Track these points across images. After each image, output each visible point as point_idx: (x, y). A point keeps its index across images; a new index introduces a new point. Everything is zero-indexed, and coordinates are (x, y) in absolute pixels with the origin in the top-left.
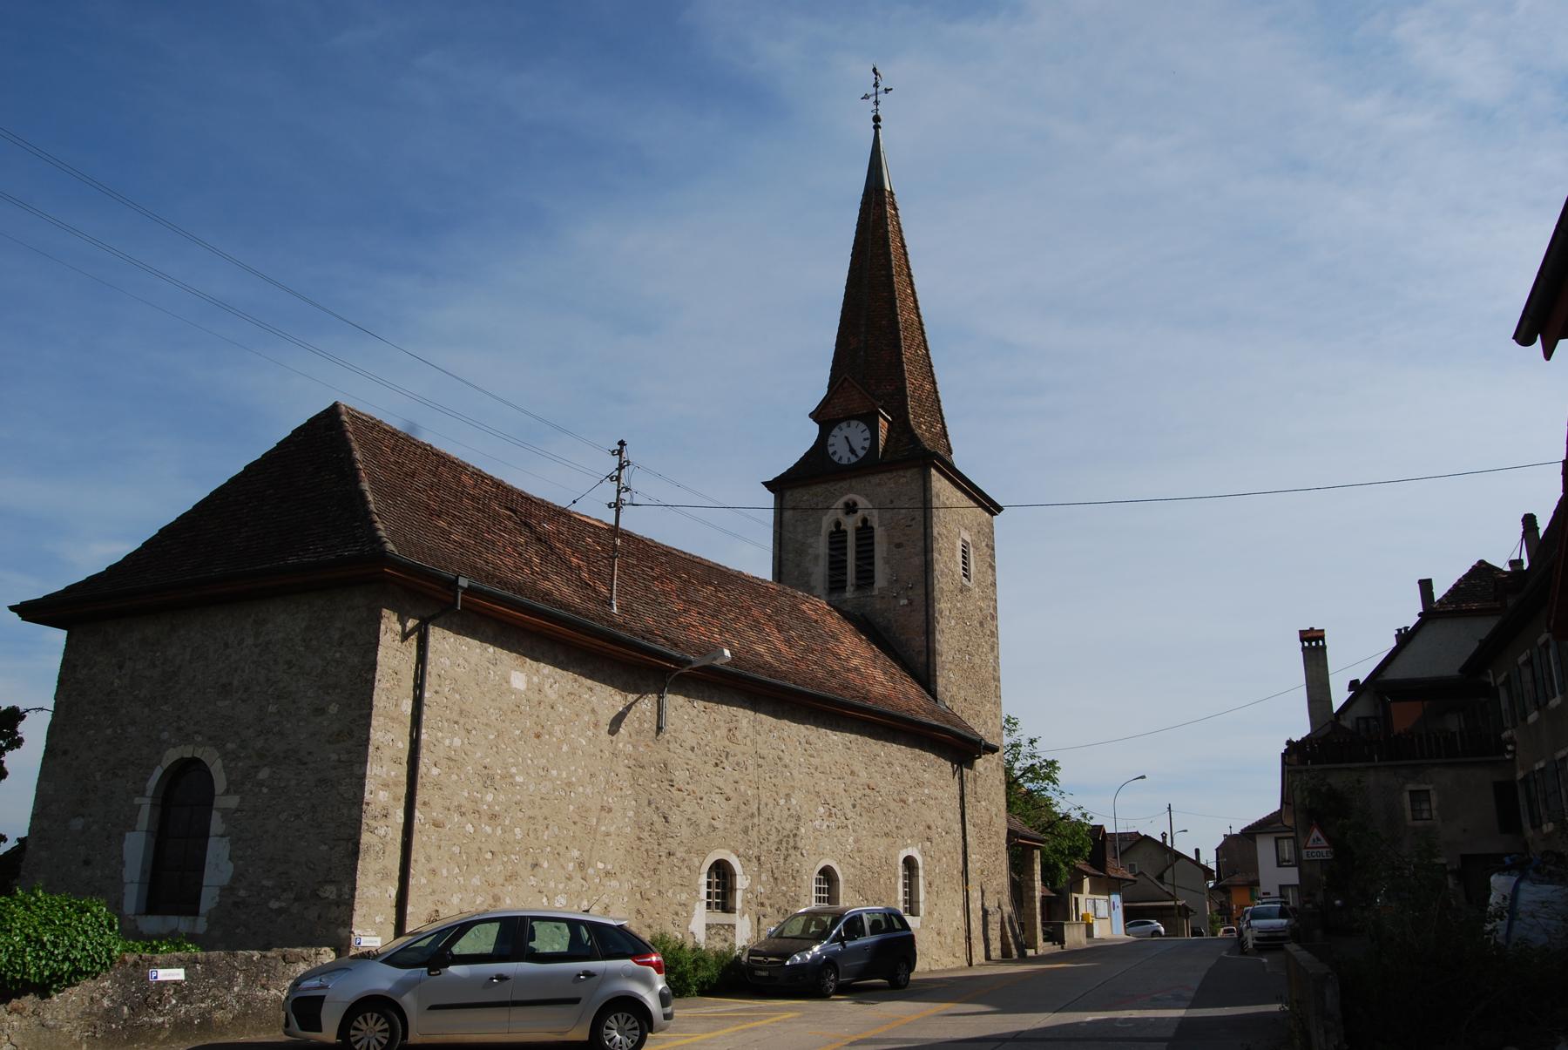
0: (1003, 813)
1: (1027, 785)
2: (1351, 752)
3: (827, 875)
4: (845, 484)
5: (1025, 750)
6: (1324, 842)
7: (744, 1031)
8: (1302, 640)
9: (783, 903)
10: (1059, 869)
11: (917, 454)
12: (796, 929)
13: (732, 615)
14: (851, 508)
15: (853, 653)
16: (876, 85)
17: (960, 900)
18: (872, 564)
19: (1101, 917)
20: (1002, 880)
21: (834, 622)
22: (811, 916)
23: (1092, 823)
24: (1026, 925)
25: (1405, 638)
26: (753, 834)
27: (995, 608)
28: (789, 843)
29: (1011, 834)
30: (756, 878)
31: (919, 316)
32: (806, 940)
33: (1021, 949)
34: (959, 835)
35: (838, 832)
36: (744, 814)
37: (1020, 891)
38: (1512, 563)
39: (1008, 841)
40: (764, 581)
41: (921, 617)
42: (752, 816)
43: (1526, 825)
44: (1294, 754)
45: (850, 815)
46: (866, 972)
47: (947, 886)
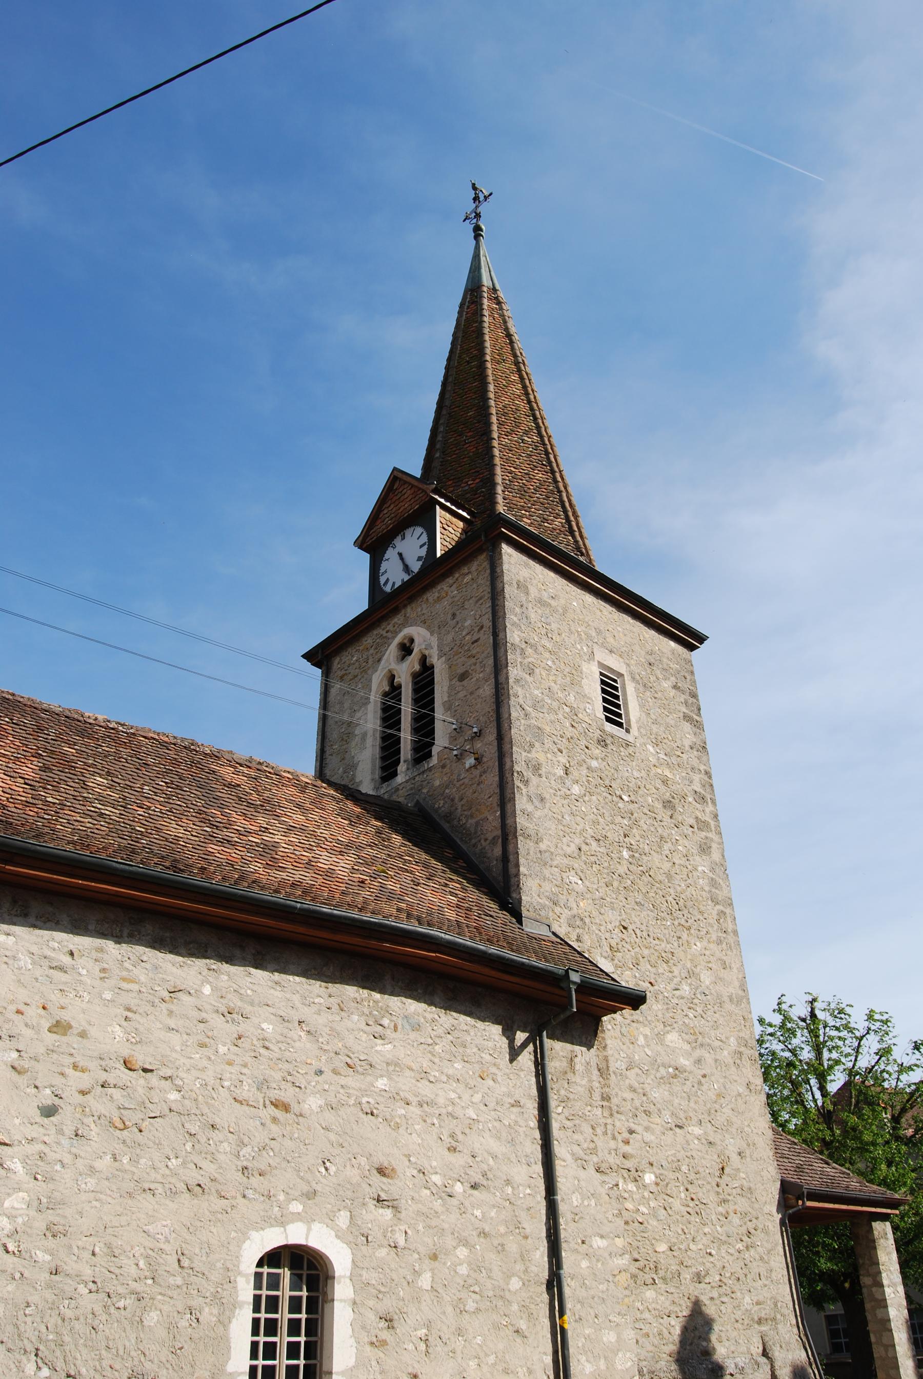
14: (406, 649)
39: (784, 1204)
41: (492, 779)
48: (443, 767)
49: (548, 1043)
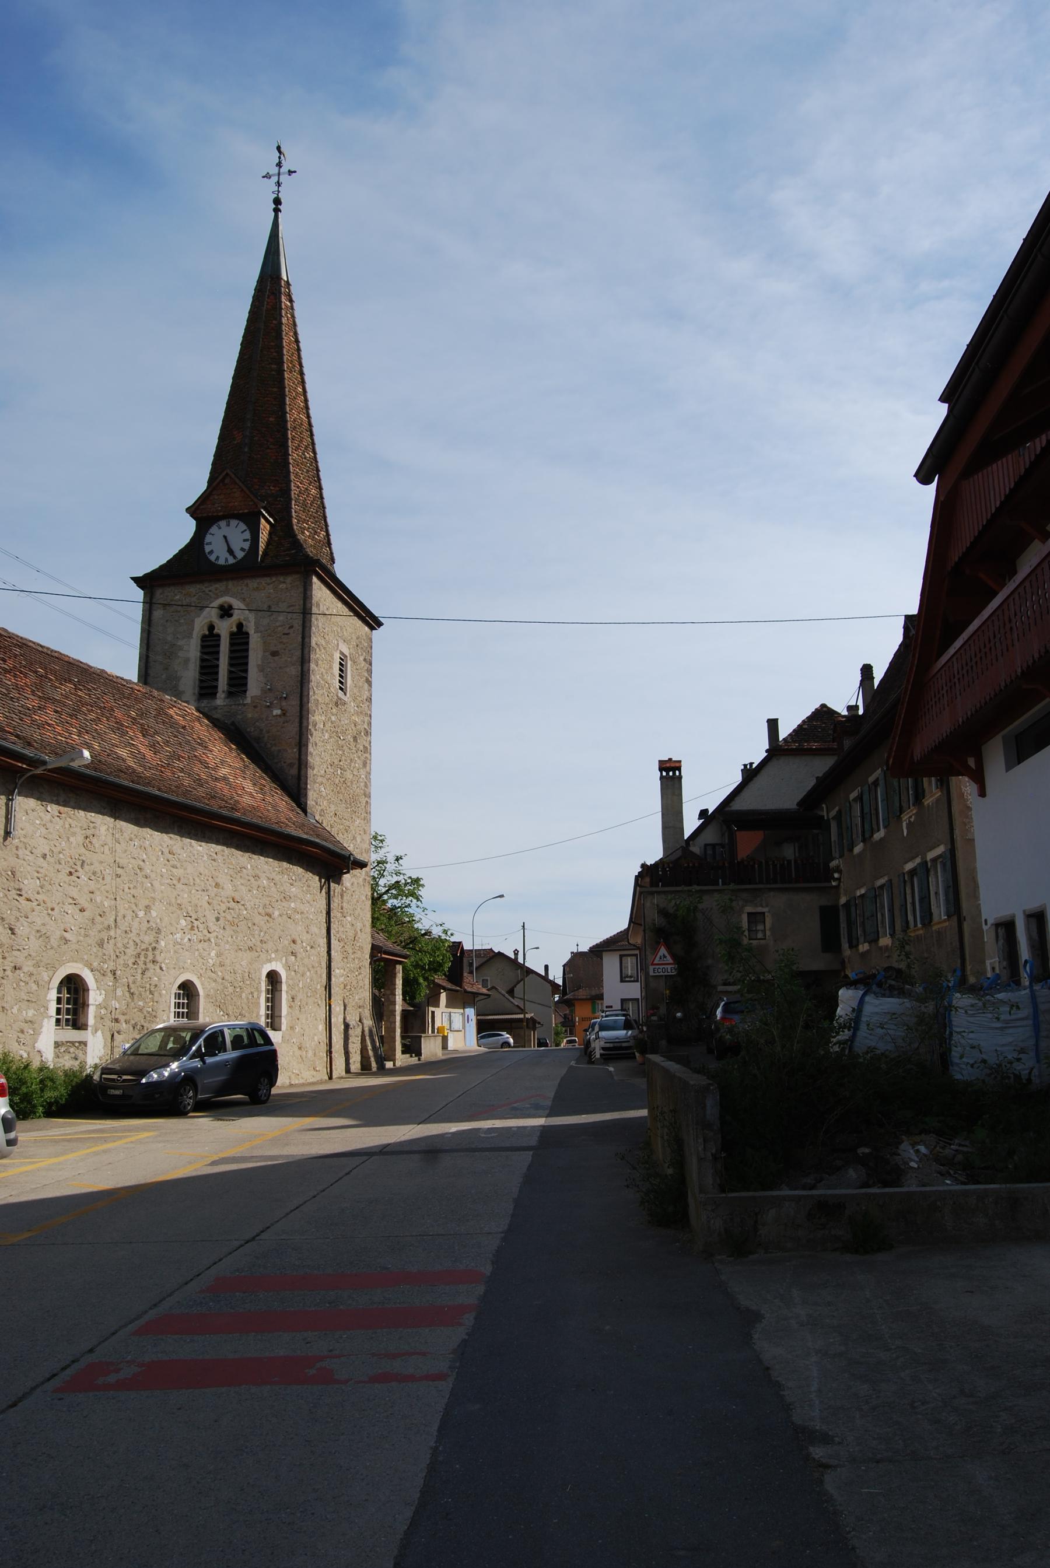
0: (368, 928)
1: (395, 902)
2: (698, 877)
3: (187, 990)
4: (220, 586)
5: (391, 867)
6: (669, 960)
7: (96, 1154)
8: (661, 770)
9: (139, 1018)
10: (419, 984)
11: (297, 561)
12: (152, 1045)
13: (93, 716)
14: (226, 612)
15: (222, 762)
16: (279, 165)
17: (322, 1014)
18: (246, 671)
19: (455, 1029)
20: (364, 994)
21: (202, 729)
22: (169, 1031)
23: (453, 939)
24: (386, 1040)
25: (750, 773)
26: (109, 948)
27: (370, 724)
28: (148, 957)
29: (375, 949)
30: (111, 993)
31: (309, 417)
32: (164, 1056)
33: (381, 1061)
34: (324, 949)
35: (200, 946)
36: (99, 927)
37: (380, 1008)
38: (850, 708)
39: (372, 956)
40: (129, 682)
41: (293, 729)
42: (109, 928)
43: (845, 945)
44: (649, 879)
45: (213, 928)
46: (227, 1088)
47: (310, 1001)
48: (255, 707)
49: (332, 884)
